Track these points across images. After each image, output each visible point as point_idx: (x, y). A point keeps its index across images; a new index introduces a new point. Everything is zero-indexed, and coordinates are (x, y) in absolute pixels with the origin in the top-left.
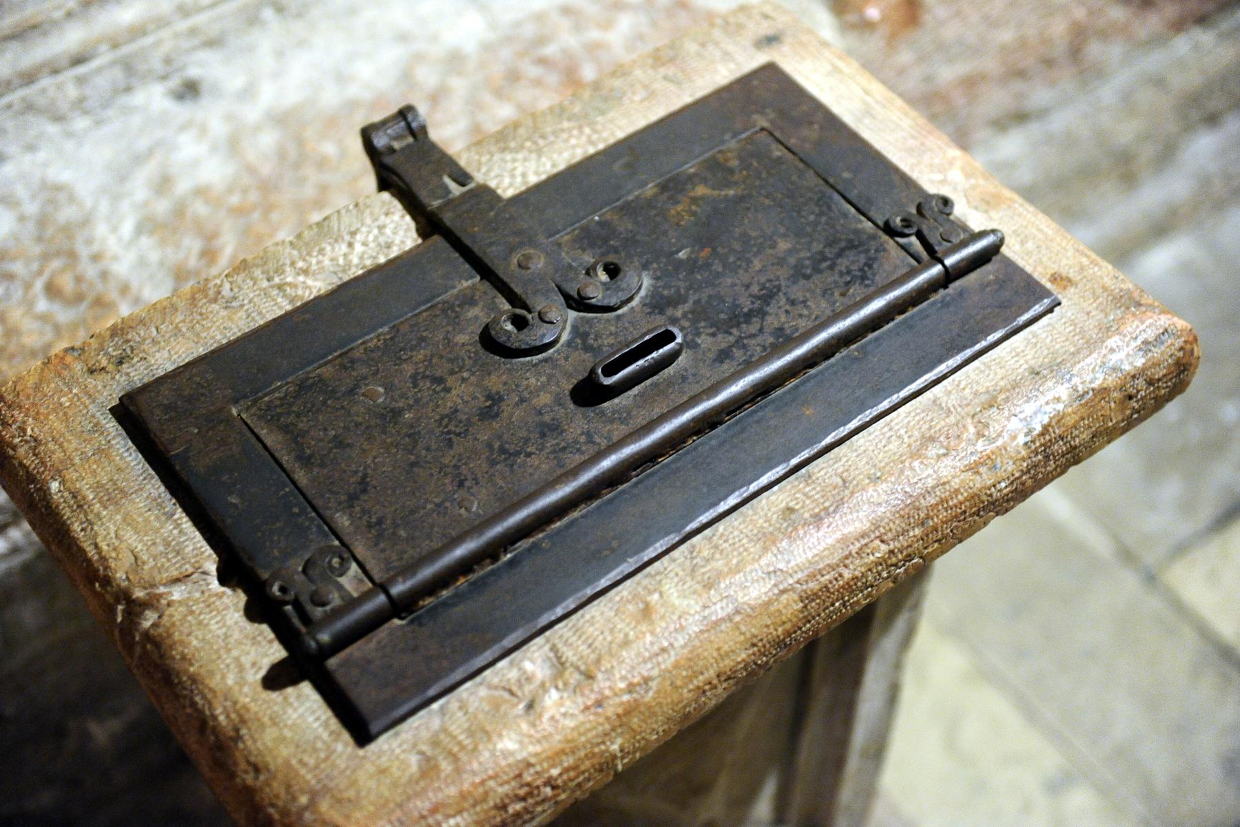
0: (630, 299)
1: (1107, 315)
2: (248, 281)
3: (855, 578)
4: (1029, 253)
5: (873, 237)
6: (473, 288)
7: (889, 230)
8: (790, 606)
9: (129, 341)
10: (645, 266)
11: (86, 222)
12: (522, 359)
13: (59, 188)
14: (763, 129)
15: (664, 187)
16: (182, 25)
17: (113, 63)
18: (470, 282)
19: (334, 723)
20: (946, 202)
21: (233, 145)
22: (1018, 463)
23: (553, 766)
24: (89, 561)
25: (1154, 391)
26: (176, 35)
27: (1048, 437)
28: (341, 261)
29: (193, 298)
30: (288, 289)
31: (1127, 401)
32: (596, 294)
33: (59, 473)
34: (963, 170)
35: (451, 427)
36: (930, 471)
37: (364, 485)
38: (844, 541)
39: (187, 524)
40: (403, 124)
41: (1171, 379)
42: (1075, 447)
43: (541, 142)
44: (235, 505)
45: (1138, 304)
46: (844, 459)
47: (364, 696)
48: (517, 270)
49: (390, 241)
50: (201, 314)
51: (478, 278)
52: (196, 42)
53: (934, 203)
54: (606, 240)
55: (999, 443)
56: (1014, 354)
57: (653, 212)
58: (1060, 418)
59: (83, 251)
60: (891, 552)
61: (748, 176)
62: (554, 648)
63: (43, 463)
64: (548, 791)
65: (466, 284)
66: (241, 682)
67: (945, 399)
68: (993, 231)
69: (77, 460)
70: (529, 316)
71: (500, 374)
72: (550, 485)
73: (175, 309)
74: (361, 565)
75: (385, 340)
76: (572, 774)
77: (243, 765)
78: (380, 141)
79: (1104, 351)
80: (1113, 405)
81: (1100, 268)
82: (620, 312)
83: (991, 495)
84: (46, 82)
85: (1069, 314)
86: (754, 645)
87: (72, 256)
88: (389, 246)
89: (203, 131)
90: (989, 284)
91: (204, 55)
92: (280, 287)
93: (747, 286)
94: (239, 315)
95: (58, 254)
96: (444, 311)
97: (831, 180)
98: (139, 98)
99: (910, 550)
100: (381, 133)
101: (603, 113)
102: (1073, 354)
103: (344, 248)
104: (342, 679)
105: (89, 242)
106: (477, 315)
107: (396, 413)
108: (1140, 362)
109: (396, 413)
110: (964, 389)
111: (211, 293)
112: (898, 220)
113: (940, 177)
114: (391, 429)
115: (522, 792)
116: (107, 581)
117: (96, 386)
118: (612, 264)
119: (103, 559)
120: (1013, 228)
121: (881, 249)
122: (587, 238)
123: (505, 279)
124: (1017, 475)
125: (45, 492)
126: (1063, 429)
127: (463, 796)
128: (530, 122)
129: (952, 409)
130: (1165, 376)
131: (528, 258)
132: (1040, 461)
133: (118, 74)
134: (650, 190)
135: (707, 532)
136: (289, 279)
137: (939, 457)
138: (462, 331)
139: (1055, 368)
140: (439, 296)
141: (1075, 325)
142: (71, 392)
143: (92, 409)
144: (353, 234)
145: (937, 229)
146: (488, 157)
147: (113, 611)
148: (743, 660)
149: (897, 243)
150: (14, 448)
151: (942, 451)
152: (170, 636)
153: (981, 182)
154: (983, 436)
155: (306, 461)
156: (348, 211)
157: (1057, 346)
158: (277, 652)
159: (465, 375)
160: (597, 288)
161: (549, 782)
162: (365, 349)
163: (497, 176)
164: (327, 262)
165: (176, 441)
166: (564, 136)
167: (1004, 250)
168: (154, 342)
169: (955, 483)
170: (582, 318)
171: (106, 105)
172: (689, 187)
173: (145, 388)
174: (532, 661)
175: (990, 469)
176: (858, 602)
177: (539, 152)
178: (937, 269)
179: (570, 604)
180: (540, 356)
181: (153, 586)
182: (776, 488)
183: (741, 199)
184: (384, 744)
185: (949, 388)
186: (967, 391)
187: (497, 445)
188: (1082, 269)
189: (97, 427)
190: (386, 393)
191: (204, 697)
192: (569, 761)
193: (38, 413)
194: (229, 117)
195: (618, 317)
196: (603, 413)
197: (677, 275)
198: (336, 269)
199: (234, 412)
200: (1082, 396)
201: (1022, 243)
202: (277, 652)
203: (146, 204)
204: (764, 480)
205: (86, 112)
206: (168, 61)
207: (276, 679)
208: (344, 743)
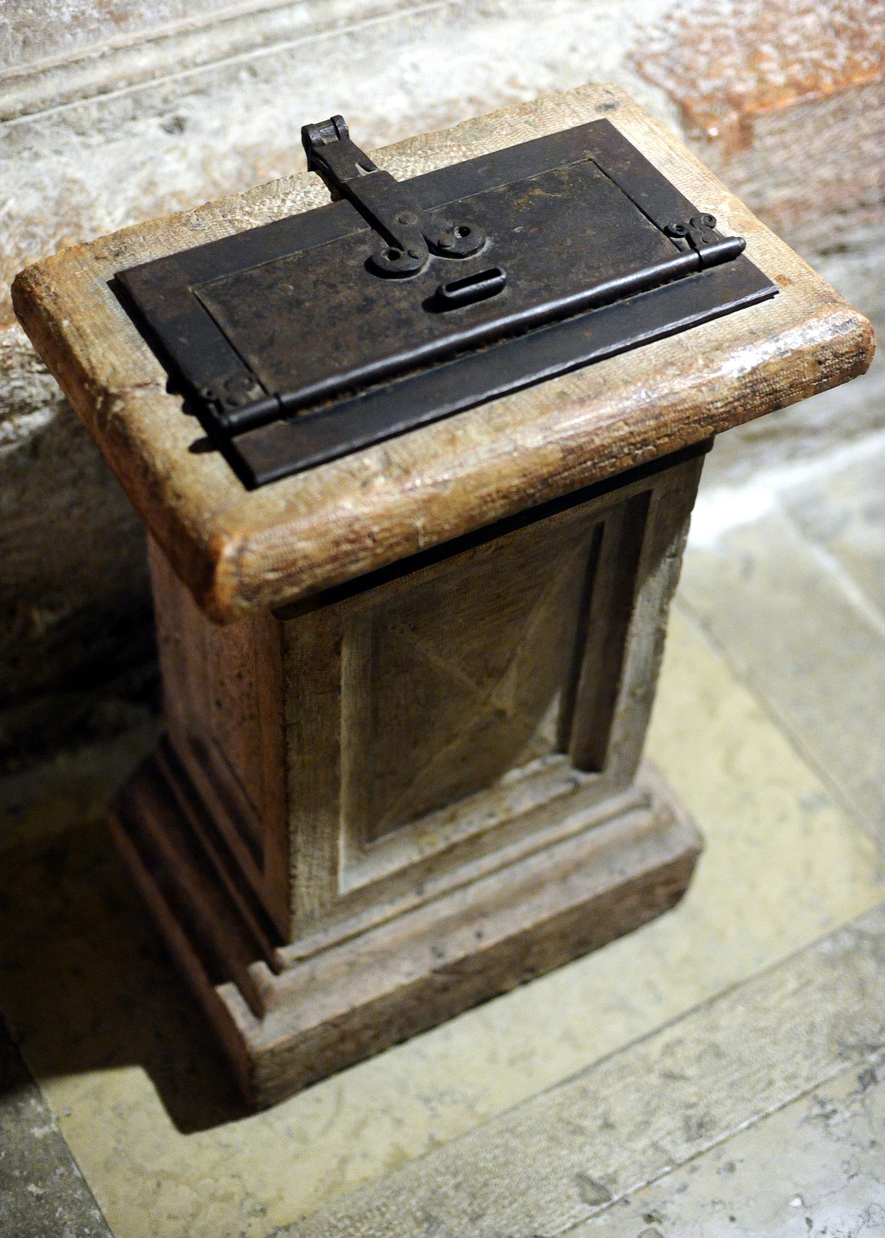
0: (474, 251)
1: (811, 305)
2: (210, 216)
3: (603, 446)
4: (765, 261)
5: (656, 235)
6: (365, 234)
7: (668, 232)
8: (555, 455)
9: (124, 243)
10: (489, 234)
11: (91, 206)
12: (392, 280)
13: (75, 181)
14: (590, 160)
15: (512, 188)
16: (180, 75)
17: (126, 96)
18: (363, 230)
19: (233, 477)
20: (711, 218)
21: (204, 166)
22: (731, 390)
23: (375, 524)
24: (82, 369)
25: (838, 363)
26: (175, 82)
27: (755, 377)
28: (275, 210)
29: (171, 221)
30: (236, 223)
31: (818, 366)
32: (452, 246)
33: (69, 316)
34: (730, 205)
35: (337, 315)
36: (666, 384)
37: (271, 341)
38: (599, 418)
39: (150, 354)
40: (332, 127)
41: (852, 357)
42: (776, 391)
43: (429, 152)
44: (184, 344)
45: (835, 301)
46: (607, 369)
47: (254, 460)
48: (398, 224)
49: (311, 201)
50: (175, 232)
51: (370, 228)
52: (187, 89)
53: (702, 218)
54: (465, 215)
55: (719, 374)
56: (740, 320)
57: (501, 202)
58: (766, 365)
59: (86, 225)
60: (631, 433)
61: (574, 187)
62: (386, 454)
63: (60, 309)
64: (369, 542)
65: (360, 231)
66: (175, 447)
67: (687, 341)
68: (739, 238)
69: (82, 309)
70: (401, 253)
71: (375, 287)
72: (398, 352)
73: (157, 226)
74: (263, 387)
75: (299, 258)
76: (387, 534)
77: (170, 494)
78: (314, 137)
79: (805, 327)
80: (806, 365)
81: (813, 276)
82: (466, 259)
83: (709, 410)
84: (78, 104)
85: (785, 301)
86: (525, 476)
87: (78, 226)
88: (310, 204)
89: (184, 154)
90: (731, 273)
91: (192, 100)
92: (230, 222)
93: (559, 254)
94: (201, 235)
95: (68, 225)
96: (342, 245)
97: (633, 197)
98: (139, 126)
99: (646, 436)
100: (316, 131)
101: (477, 139)
102: (782, 325)
103: (279, 202)
104: (243, 450)
105: (91, 219)
106: (365, 250)
107: (299, 303)
108: (828, 338)
109: (299, 303)
110: (700, 337)
111: (183, 220)
112: (674, 226)
113: (713, 207)
114: (295, 310)
115: (352, 536)
116: (93, 382)
117: (99, 268)
118: (465, 228)
119: (92, 368)
120: (758, 245)
121: (660, 242)
122: (451, 212)
123: (388, 229)
124: (731, 400)
125: (58, 326)
126: (767, 374)
127: (313, 529)
128: (424, 139)
129: (690, 348)
130: (847, 352)
131: (407, 217)
132: (748, 394)
133: (129, 103)
134: (501, 188)
135: (504, 399)
136: (237, 218)
137: (674, 376)
138: (354, 258)
139: (770, 333)
140: (340, 236)
141: (787, 308)
142: (82, 269)
143: (95, 280)
144: (286, 194)
145: (701, 234)
146: (390, 157)
147: (93, 401)
148: (516, 486)
149: (671, 240)
150: (41, 299)
151: (678, 372)
152: (131, 415)
153: (742, 214)
154: (708, 367)
155: (235, 324)
156: (285, 180)
157: (772, 319)
158: (199, 433)
159: (351, 285)
160: (453, 240)
161: (370, 535)
162: (284, 263)
163: (394, 170)
164: (265, 210)
165: (147, 301)
166: (447, 150)
167: (744, 253)
168: (141, 245)
169: (683, 395)
170: (439, 260)
171: (116, 127)
172: (530, 189)
173: (131, 270)
174: (370, 458)
175: (710, 390)
176: (604, 468)
177: (427, 158)
178: (695, 256)
179: (401, 426)
180: (405, 279)
181: (123, 386)
182: (556, 380)
183: (564, 201)
184: (264, 492)
185: (691, 335)
186: (703, 338)
187: (366, 328)
188: (800, 275)
189: (97, 291)
190: (295, 290)
191: (150, 453)
192: (386, 524)
193: (60, 279)
194: (204, 147)
195: (464, 262)
196: (443, 318)
197: (511, 241)
198: (271, 215)
199: (190, 289)
200: (783, 353)
201: (762, 254)
202: (199, 433)
203: (135, 198)
204: (547, 372)
205: (101, 131)
206: (165, 100)
207: (197, 448)
208: (238, 489)
